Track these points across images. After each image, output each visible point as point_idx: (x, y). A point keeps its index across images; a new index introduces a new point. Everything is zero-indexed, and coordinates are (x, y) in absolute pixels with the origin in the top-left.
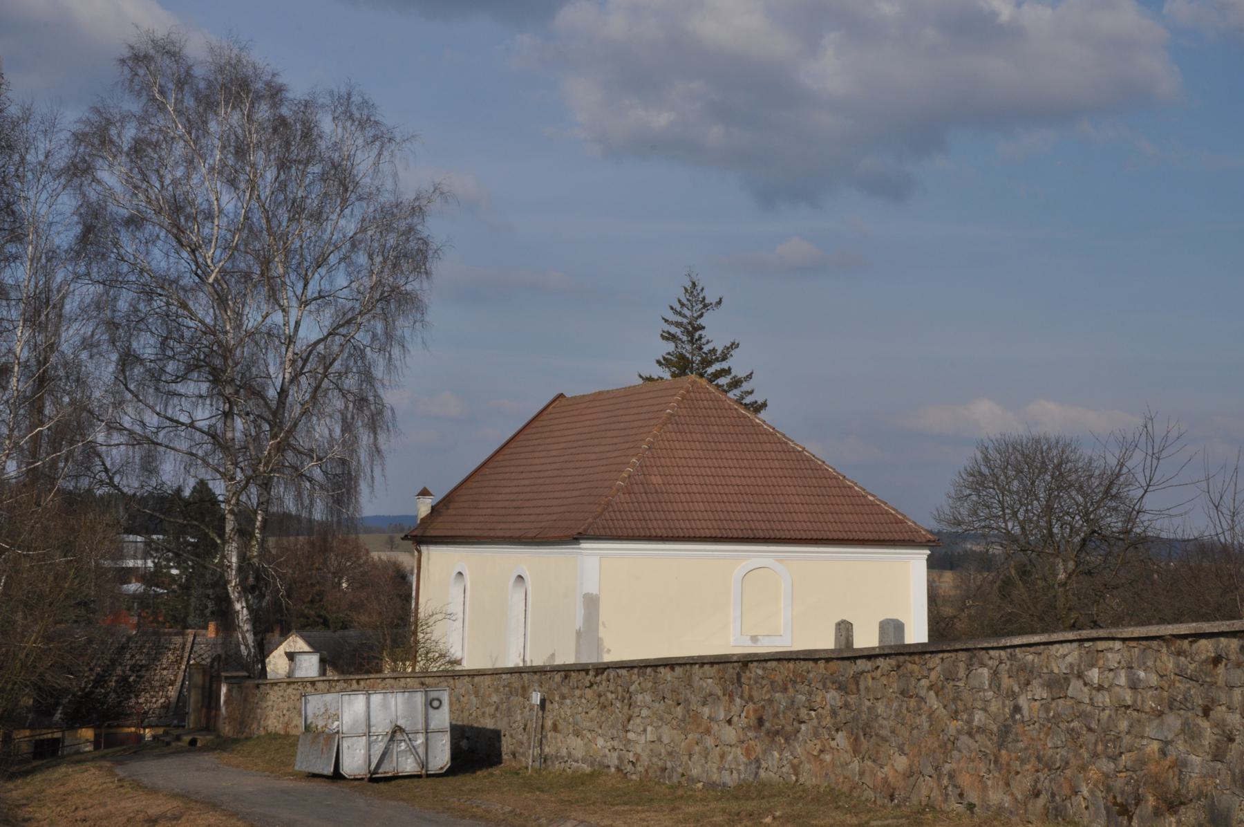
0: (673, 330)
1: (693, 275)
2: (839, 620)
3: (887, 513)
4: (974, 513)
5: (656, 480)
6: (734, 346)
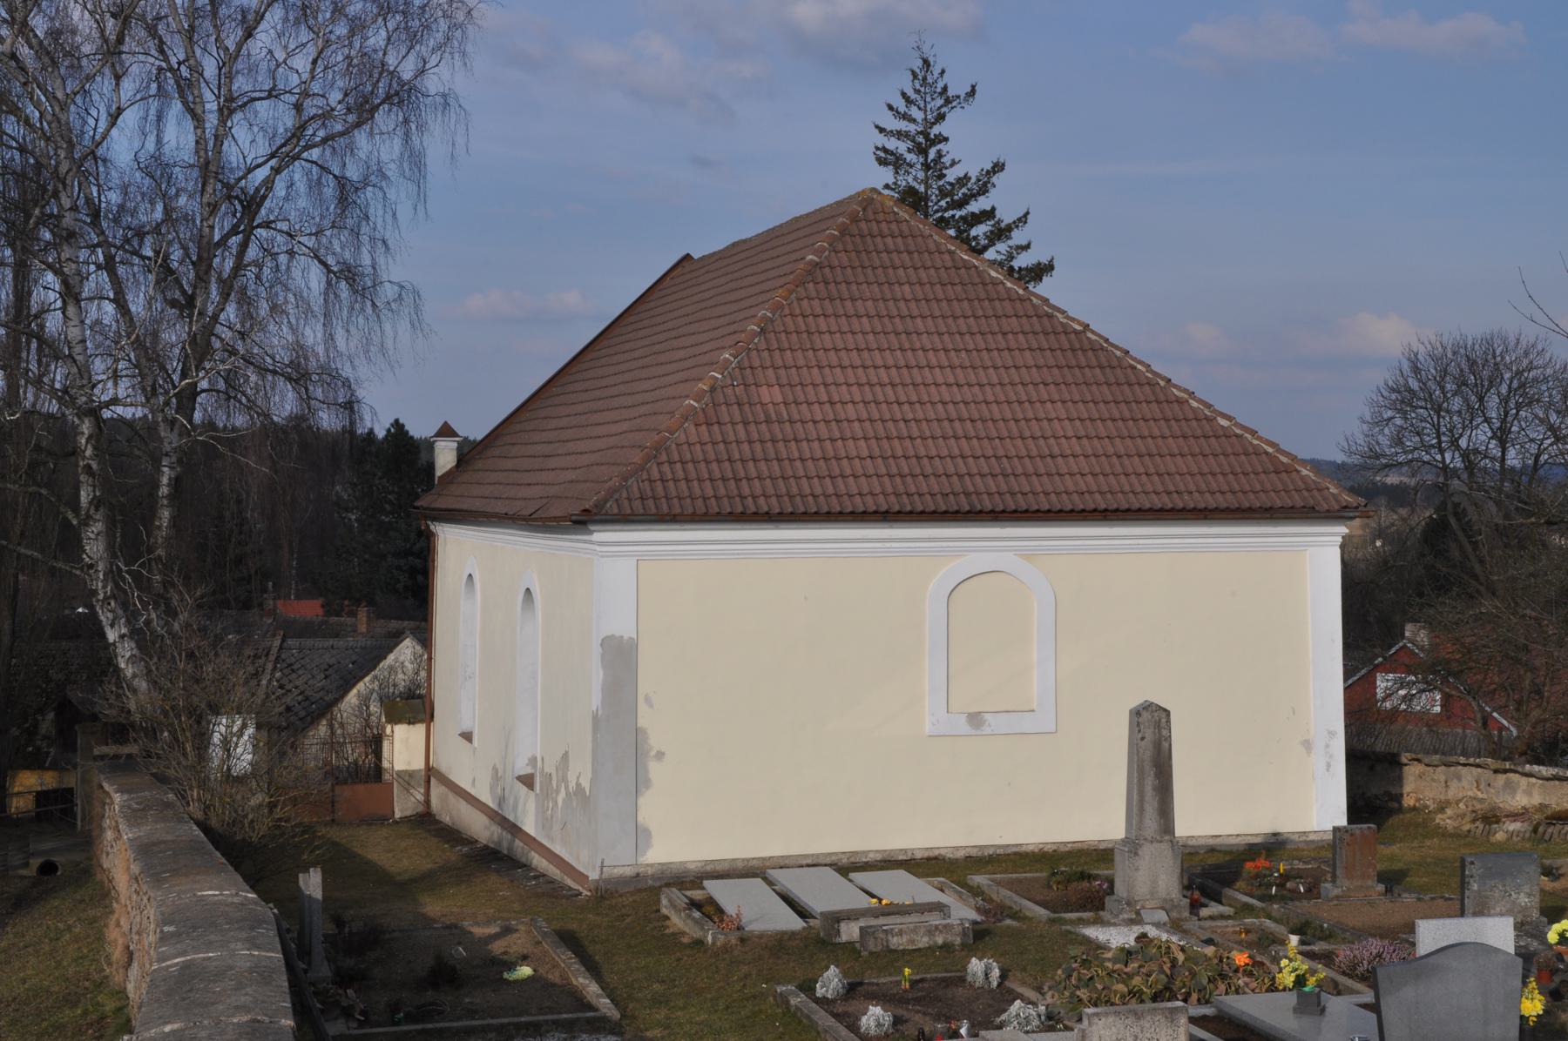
0: (892, 144)
1: (926, 48)
2: (1136, 702)
3: (1258, 452)
4: (1398, 441)
6: (998, 167)
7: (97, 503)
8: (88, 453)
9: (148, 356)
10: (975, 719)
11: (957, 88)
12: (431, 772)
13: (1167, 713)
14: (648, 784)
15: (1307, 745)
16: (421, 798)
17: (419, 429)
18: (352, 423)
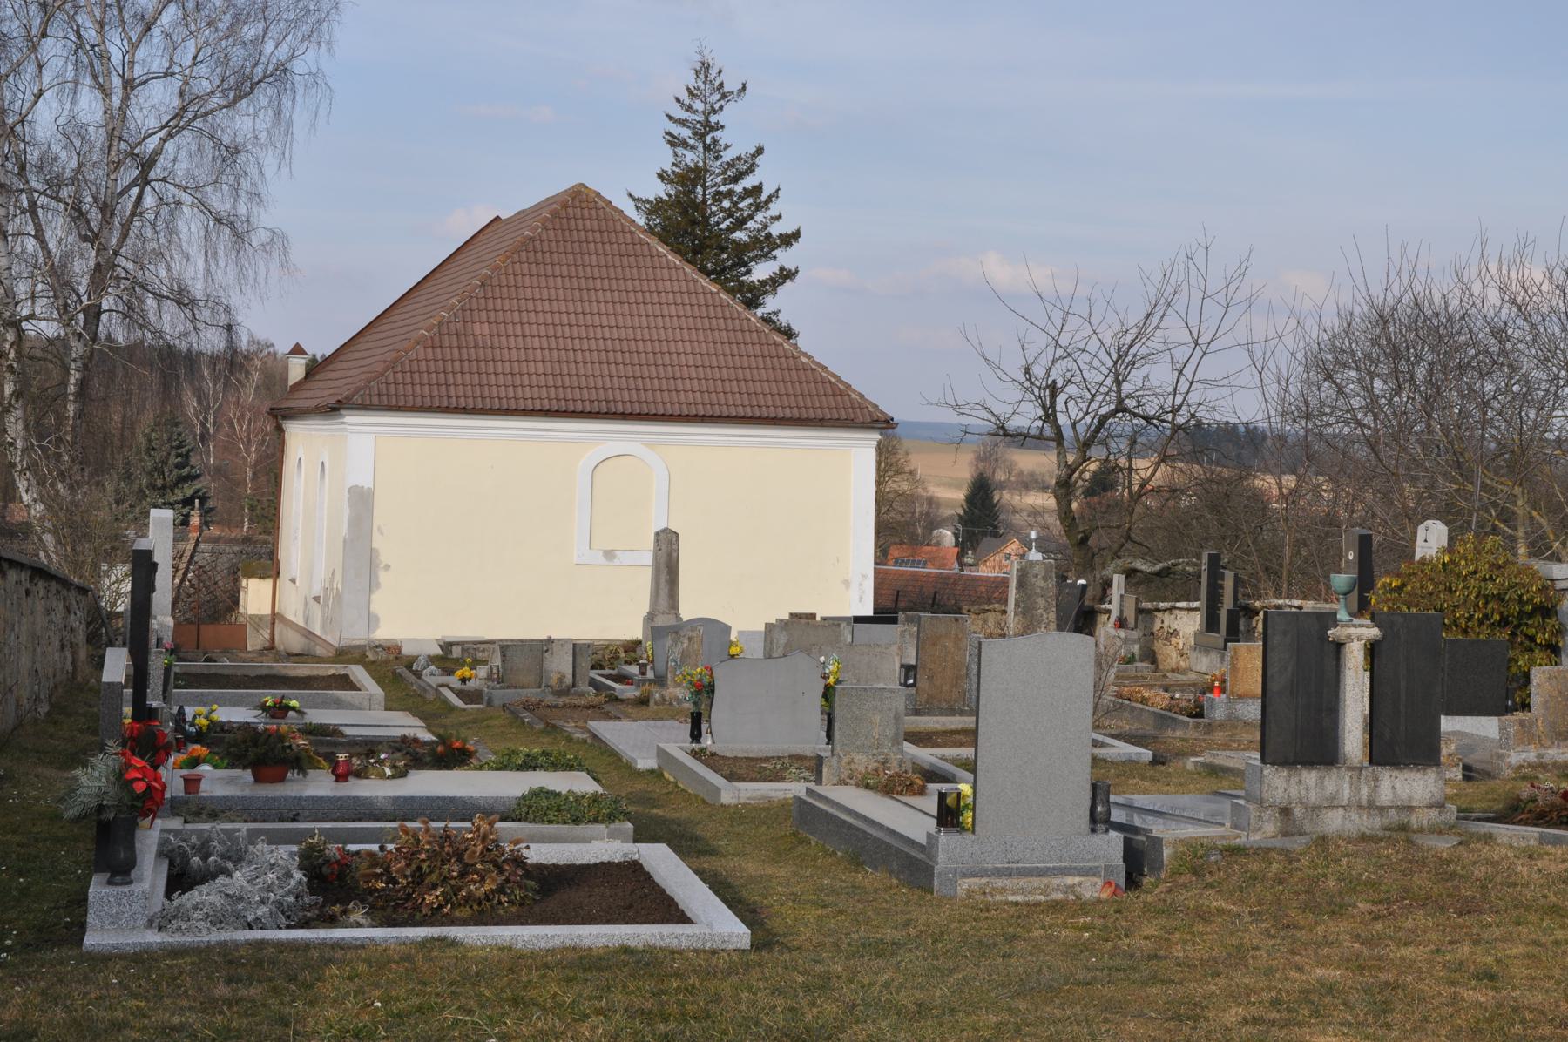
0: (678, 130)
1: (706, 52)
5: (481, 329)
6: (760, 151)
7: (17, 395)
8: (12, 355)
9: (59, 278)
10: (609, 554)
11: (731, 86)
12: (275, 617)
13: (657, 534)
14: (378, 585)
15: (847, 583)
16: (267, 636)
17: (283, 347)
18: (230, 340)
